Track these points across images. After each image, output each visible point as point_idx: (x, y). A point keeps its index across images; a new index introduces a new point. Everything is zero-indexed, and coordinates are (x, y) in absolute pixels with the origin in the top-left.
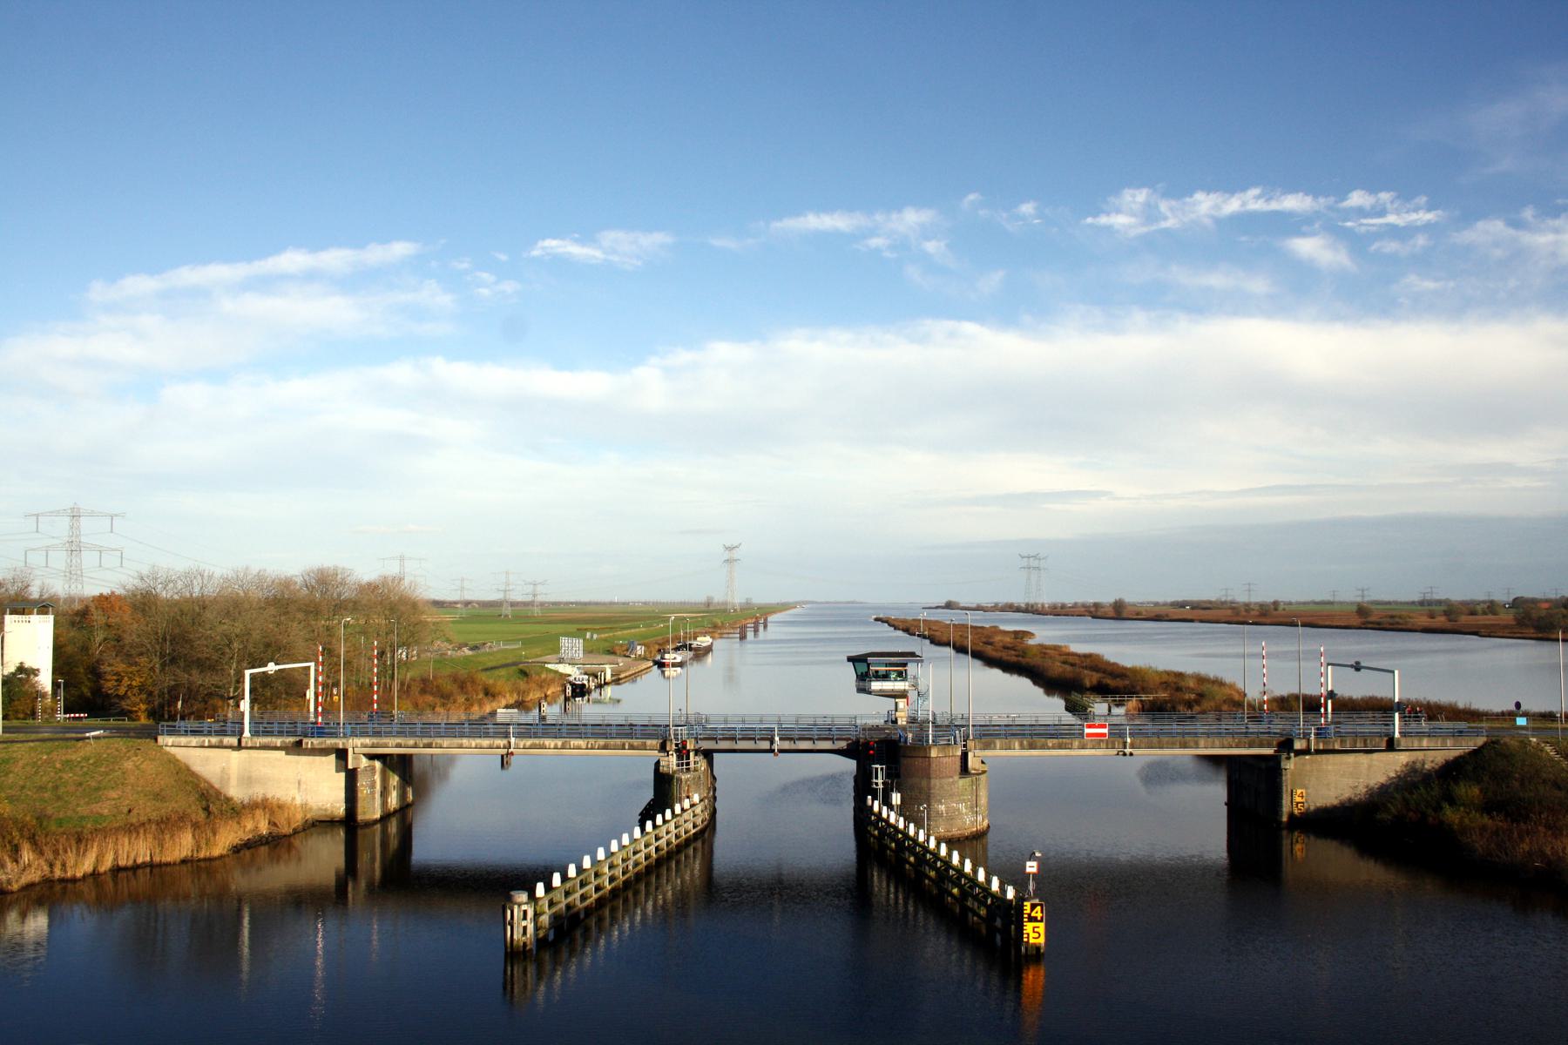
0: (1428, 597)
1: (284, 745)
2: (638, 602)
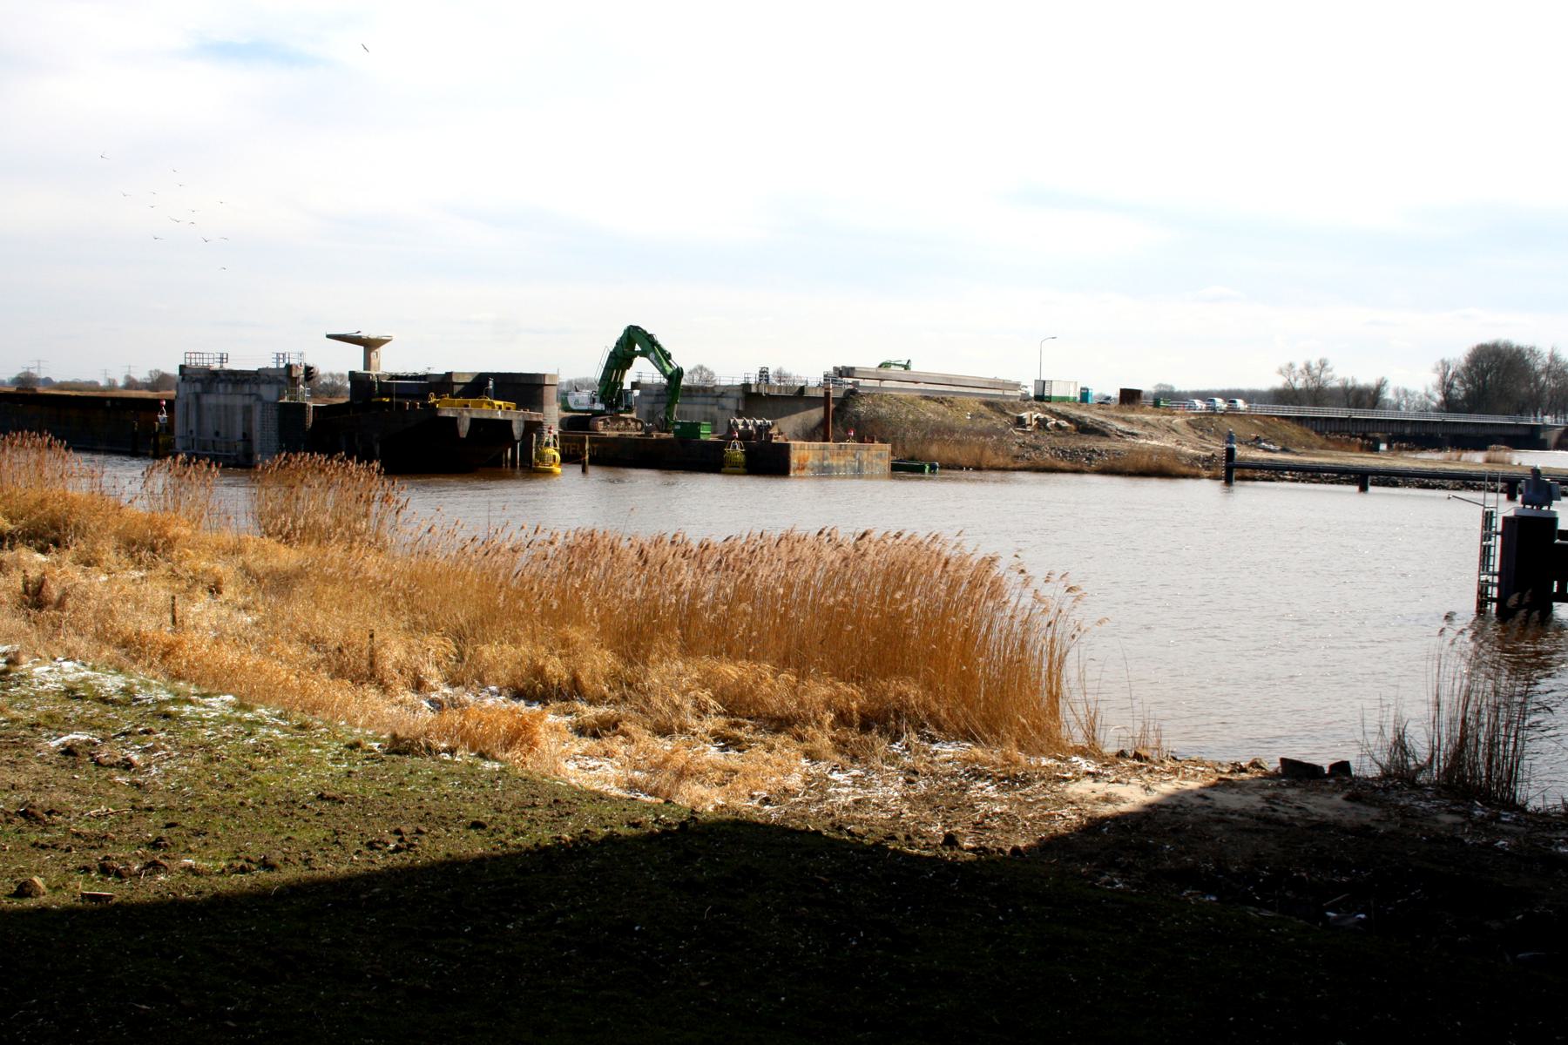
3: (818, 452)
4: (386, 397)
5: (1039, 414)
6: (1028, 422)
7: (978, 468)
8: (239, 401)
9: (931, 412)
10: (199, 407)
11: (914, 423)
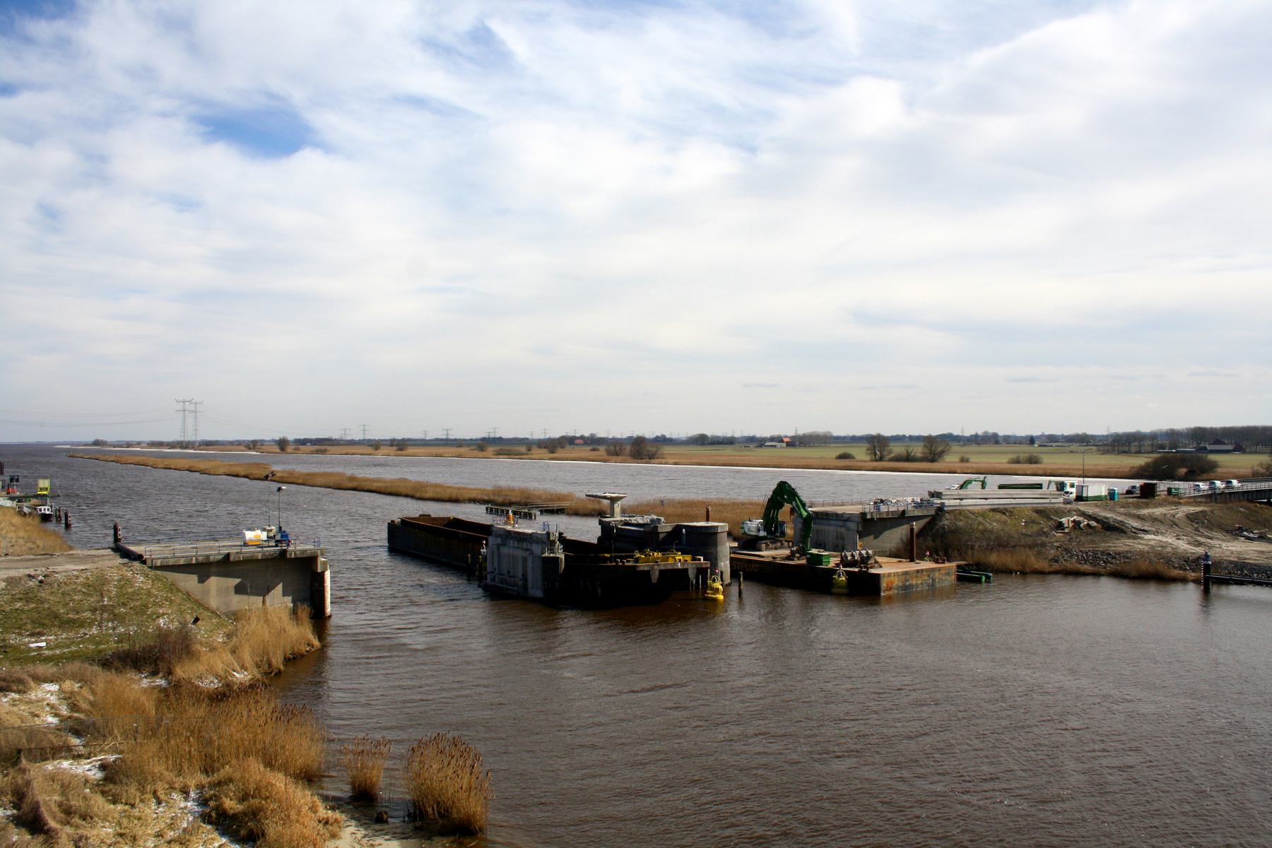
0: (492, 435)
1: (264, 557)
4: (608, 553)
5: (1075, 517)
6: (1066, 526)
7: (1024, 573)
8: (519, 553)
9: (994, 525)
10: (499, 554)
11: (983, 532)
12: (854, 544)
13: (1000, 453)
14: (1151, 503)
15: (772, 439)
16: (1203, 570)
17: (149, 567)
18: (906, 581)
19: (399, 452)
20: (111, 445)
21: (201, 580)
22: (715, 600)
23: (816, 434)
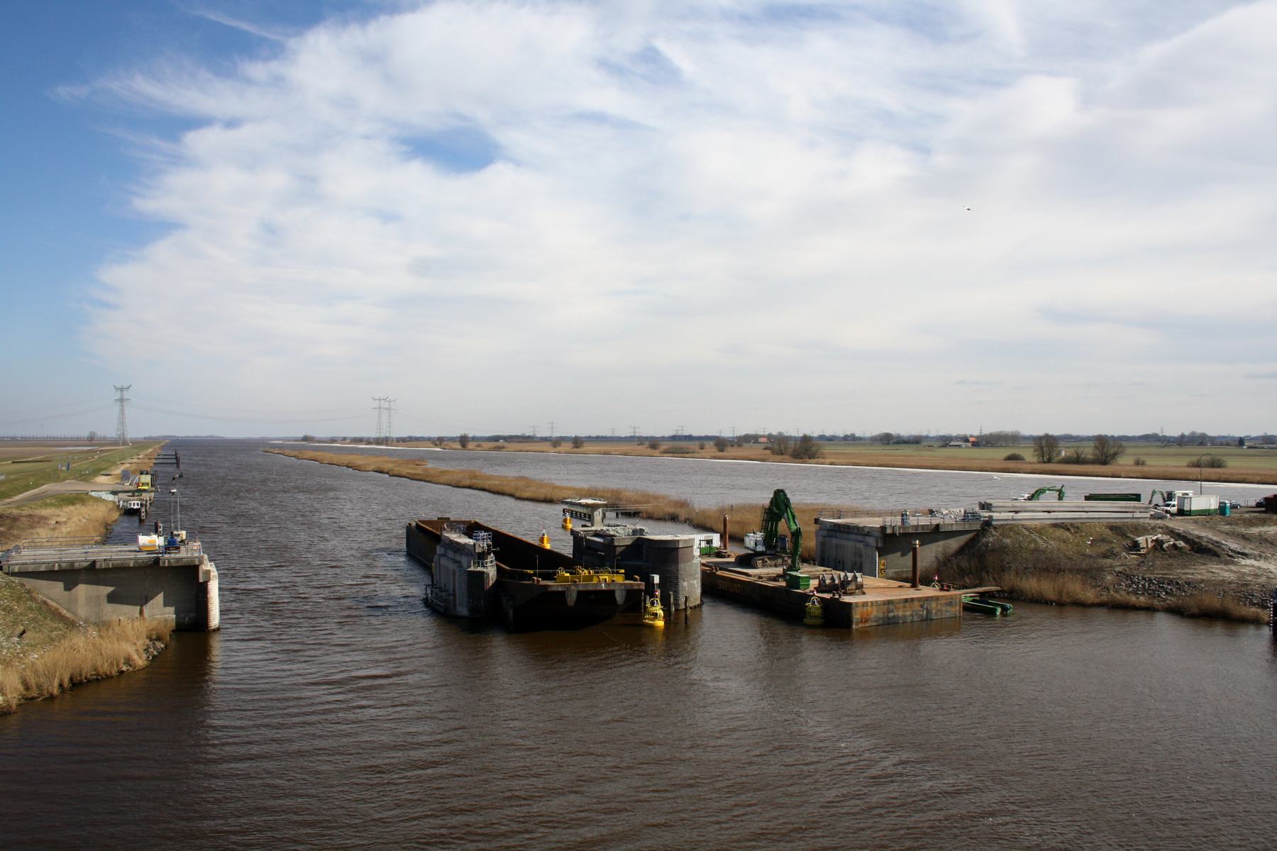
0: (680, 433)
1: (136, 565)
2: (7, 437)
3: (882, 607)
5: (1159, 536)
7: (1060, 604)
9: (1050, 544)
12: (872, 562)
13: (1181, 455)
14: (1270, 519)
15: (957, 438)
16: (1273, 611)
17: (5, 573)
18: (889, 611)
19: (575, 450)
20: (319, 442)
21: (68, 588)
22: (652, 627)
23: (1004, 434)
